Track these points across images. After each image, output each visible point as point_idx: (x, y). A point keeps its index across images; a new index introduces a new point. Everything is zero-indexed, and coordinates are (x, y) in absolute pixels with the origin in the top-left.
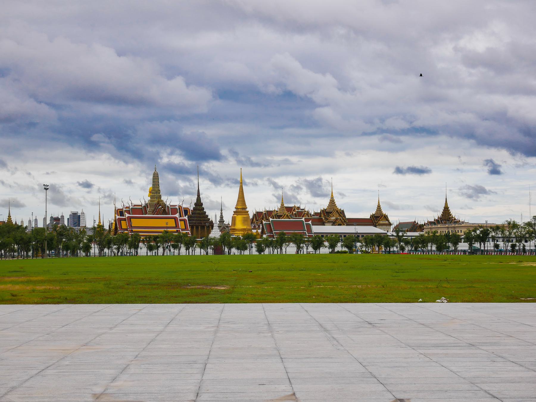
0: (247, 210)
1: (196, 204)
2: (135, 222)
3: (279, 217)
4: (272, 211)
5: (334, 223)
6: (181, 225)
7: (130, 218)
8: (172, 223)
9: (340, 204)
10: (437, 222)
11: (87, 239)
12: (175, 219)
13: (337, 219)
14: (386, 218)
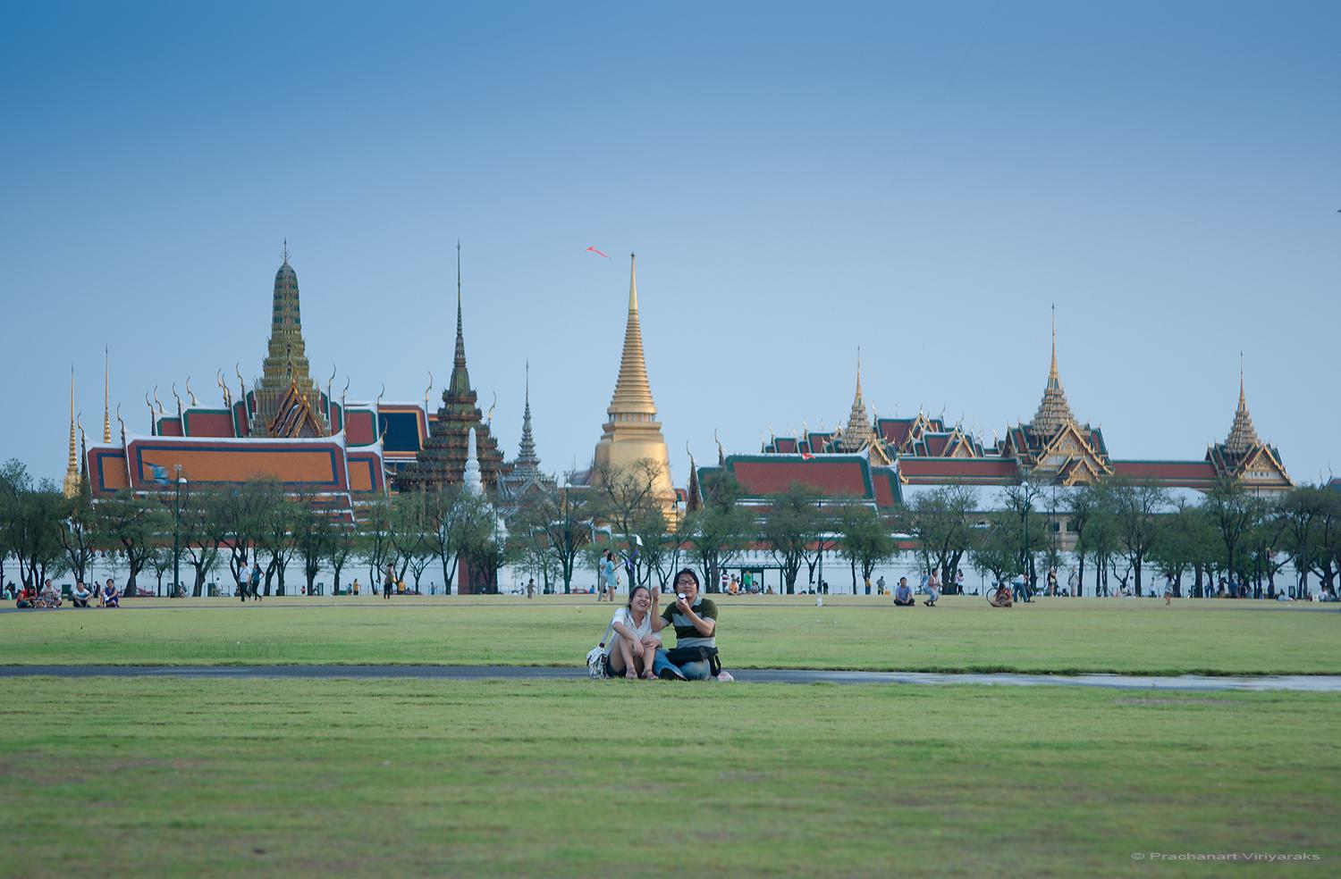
1: (449, 397)
6: (356, 476)
8: (321, 468)
9: (1083, 411)
10: (234, 418)
11: (930, 508)
12: (332, 449)
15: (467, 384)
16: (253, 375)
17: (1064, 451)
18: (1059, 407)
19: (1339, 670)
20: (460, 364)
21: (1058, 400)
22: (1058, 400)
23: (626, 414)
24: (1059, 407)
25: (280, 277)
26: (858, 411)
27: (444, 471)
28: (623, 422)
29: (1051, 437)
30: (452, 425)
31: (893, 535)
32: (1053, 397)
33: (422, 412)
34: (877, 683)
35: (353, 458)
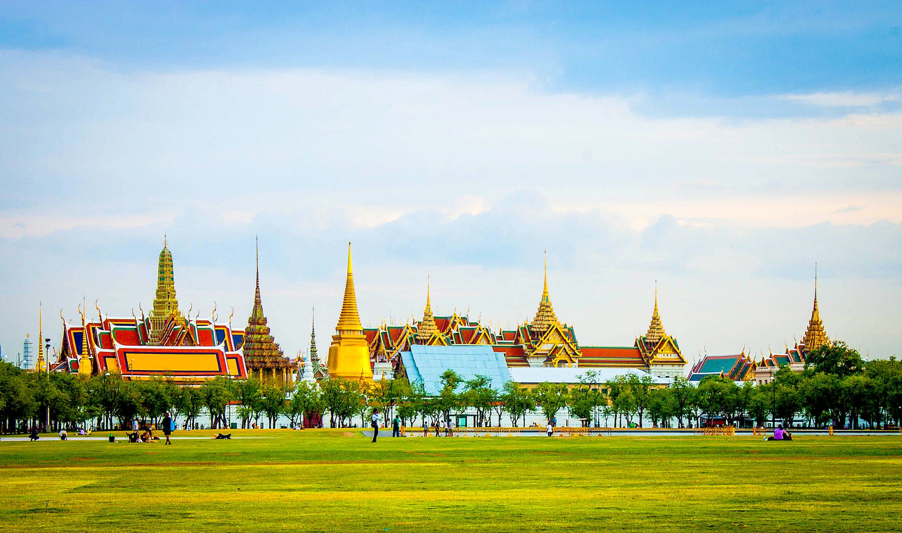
0: (285, 356)
1: (253, 321)
2: (136, 362)
4: (401, 329)
5: (549, 358)
6: (231, 368)
7: (123, 353)
8: (211, 363)
9: (563, 317)
12: (217, 353)
13: (556, 349)
14: (673, 346)
15: (262, 314)
16: (148, 311)
17: (552, 340)
18: (549, 314)
20: (258, 303)
21: (548, 309)
22: (548, 309)
24: (549, 314)
25: (163, 255)
27: (253, 362)
28: (346, 335)
29: (544, 332)
30: (255, 336)
31: (736, 382)
32: (544, 308)
33: (228, 330)
35: (229, 357)
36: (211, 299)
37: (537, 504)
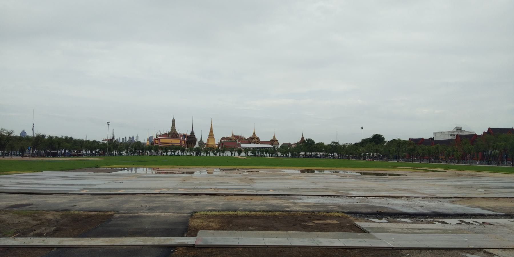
3: (231, 140)
5: (254, 143)
6: (183, 142)
7: (160, 139)
8: (178, 141)
9: (257, 135)
10: (166, 135)
12: (180, 139)
14: (277, 141)
16: (170, 130)
19: (511, 245)
23: (211, 136)
26: (303, 138)
32: (254, 134)
34: (169, 195)
36: (183, 129)
37: (332, 218)
